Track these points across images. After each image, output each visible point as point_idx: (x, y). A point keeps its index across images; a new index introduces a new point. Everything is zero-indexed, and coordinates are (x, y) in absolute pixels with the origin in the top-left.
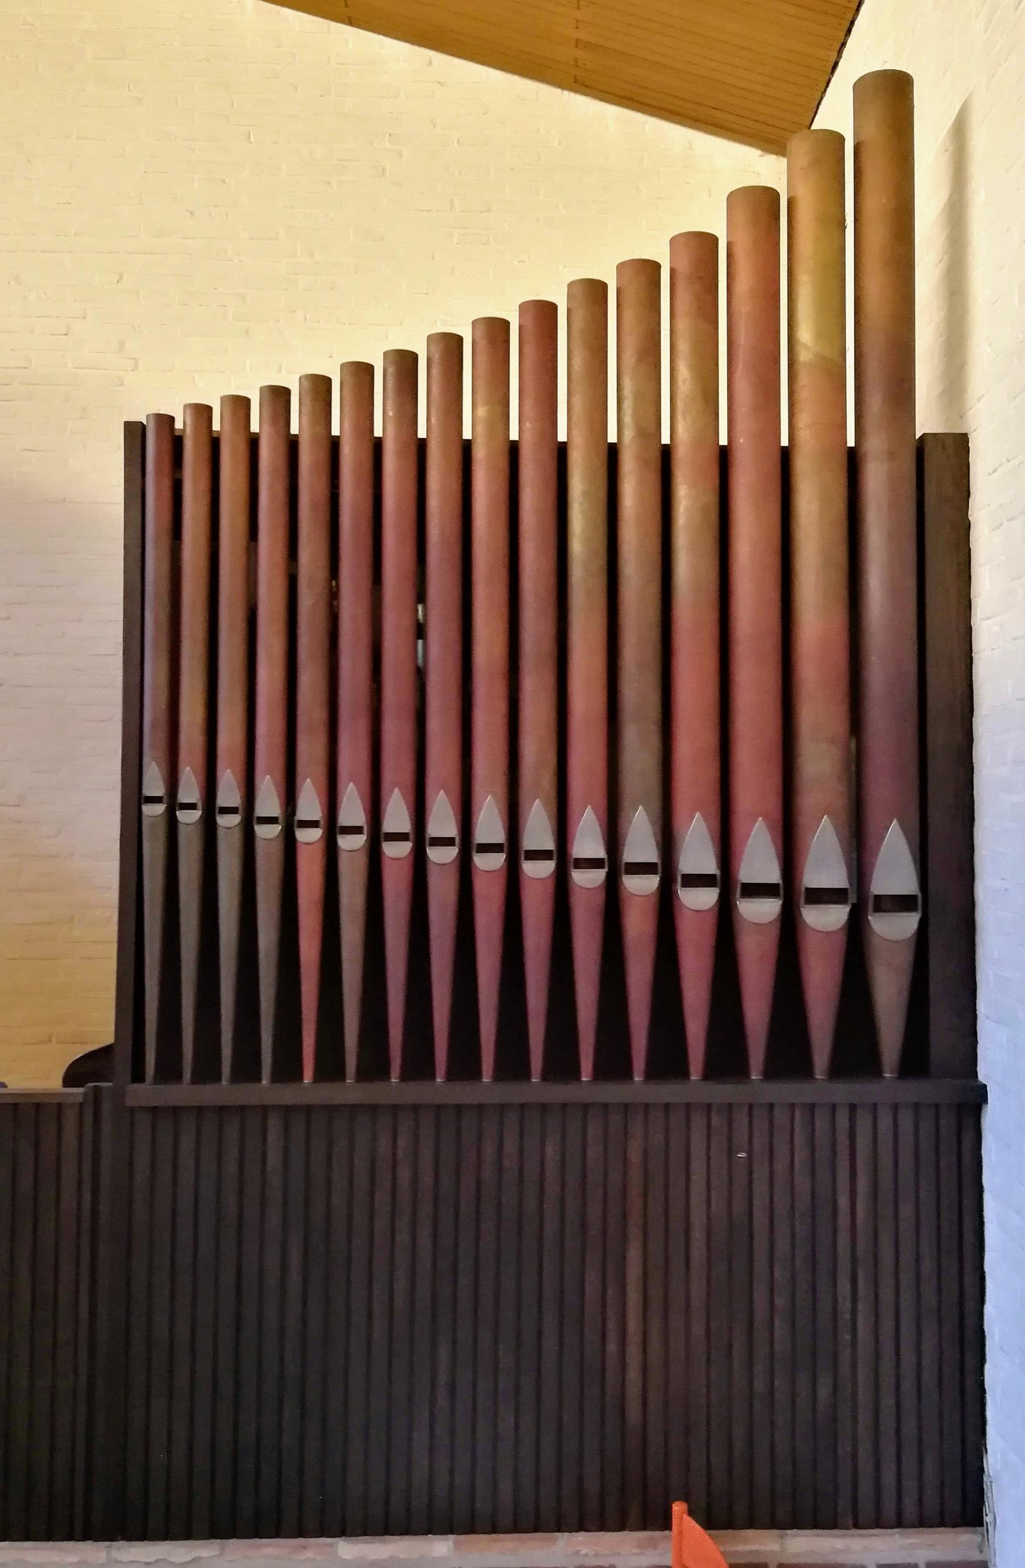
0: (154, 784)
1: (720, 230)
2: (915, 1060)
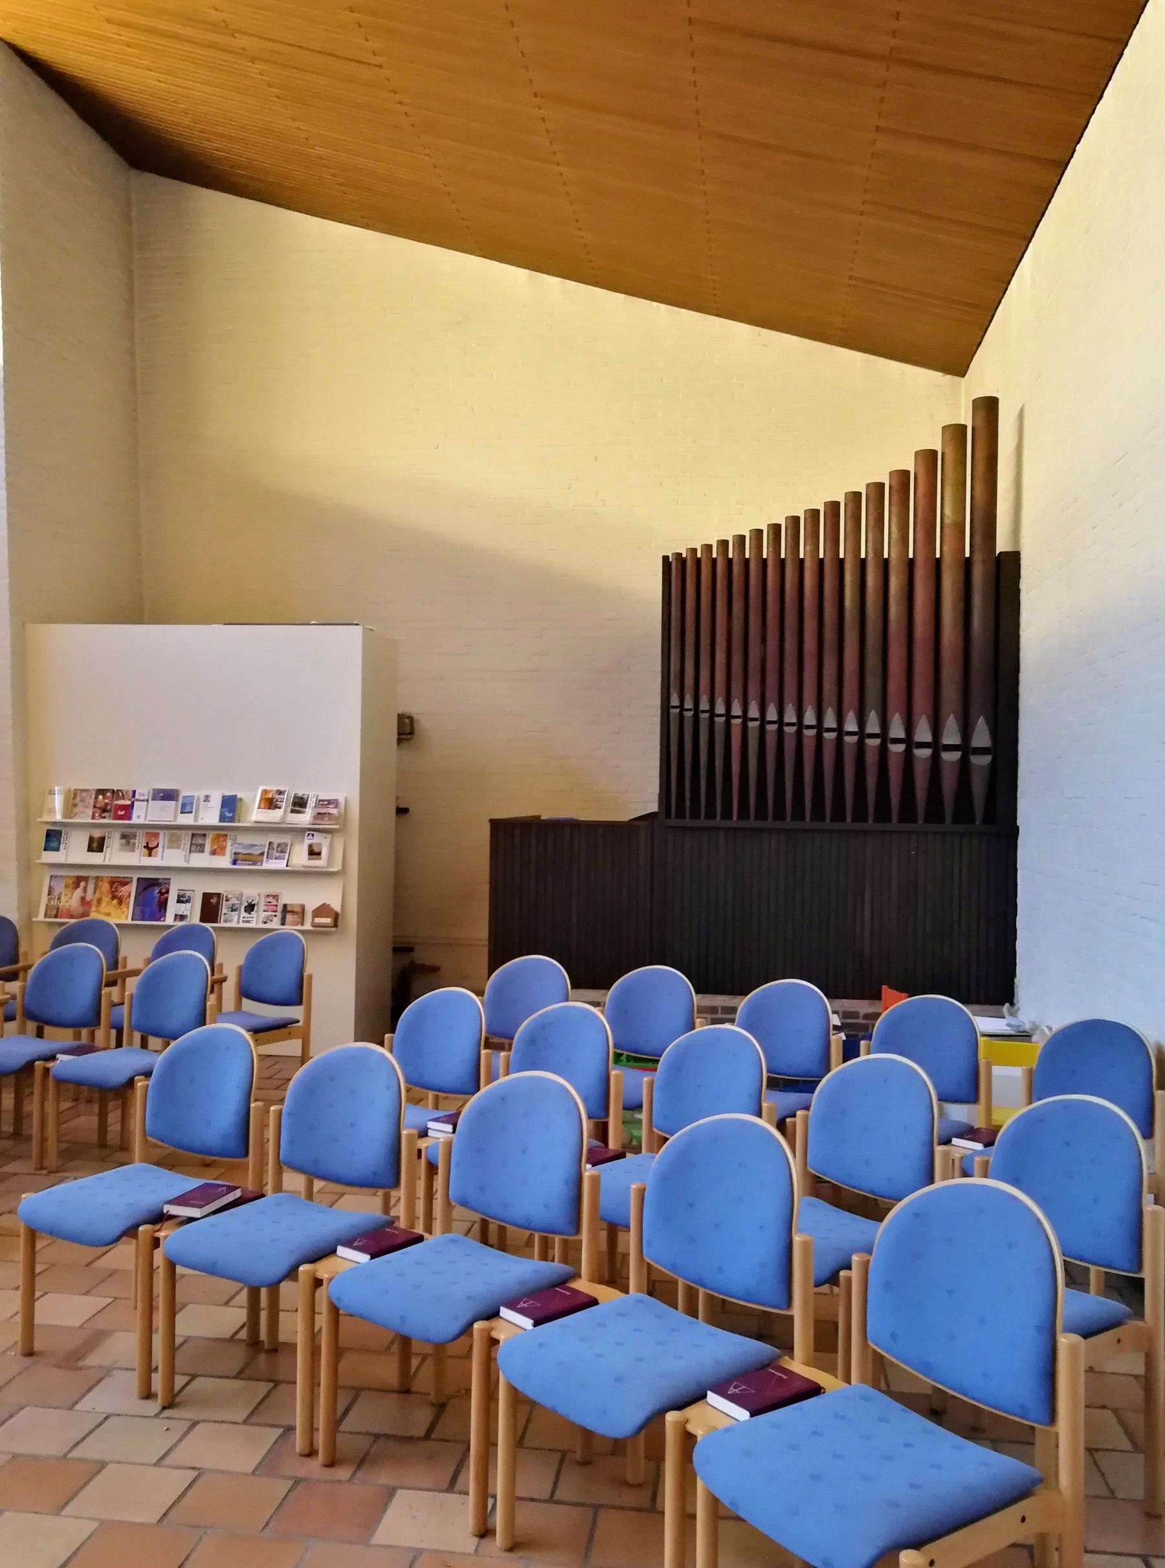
0: (675, 701)
1: (938, 448)
2: (990, 816)
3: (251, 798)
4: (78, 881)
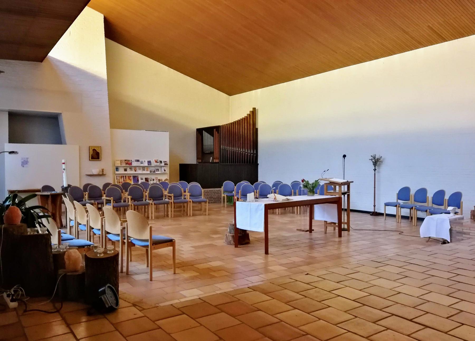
4: (122, 177)
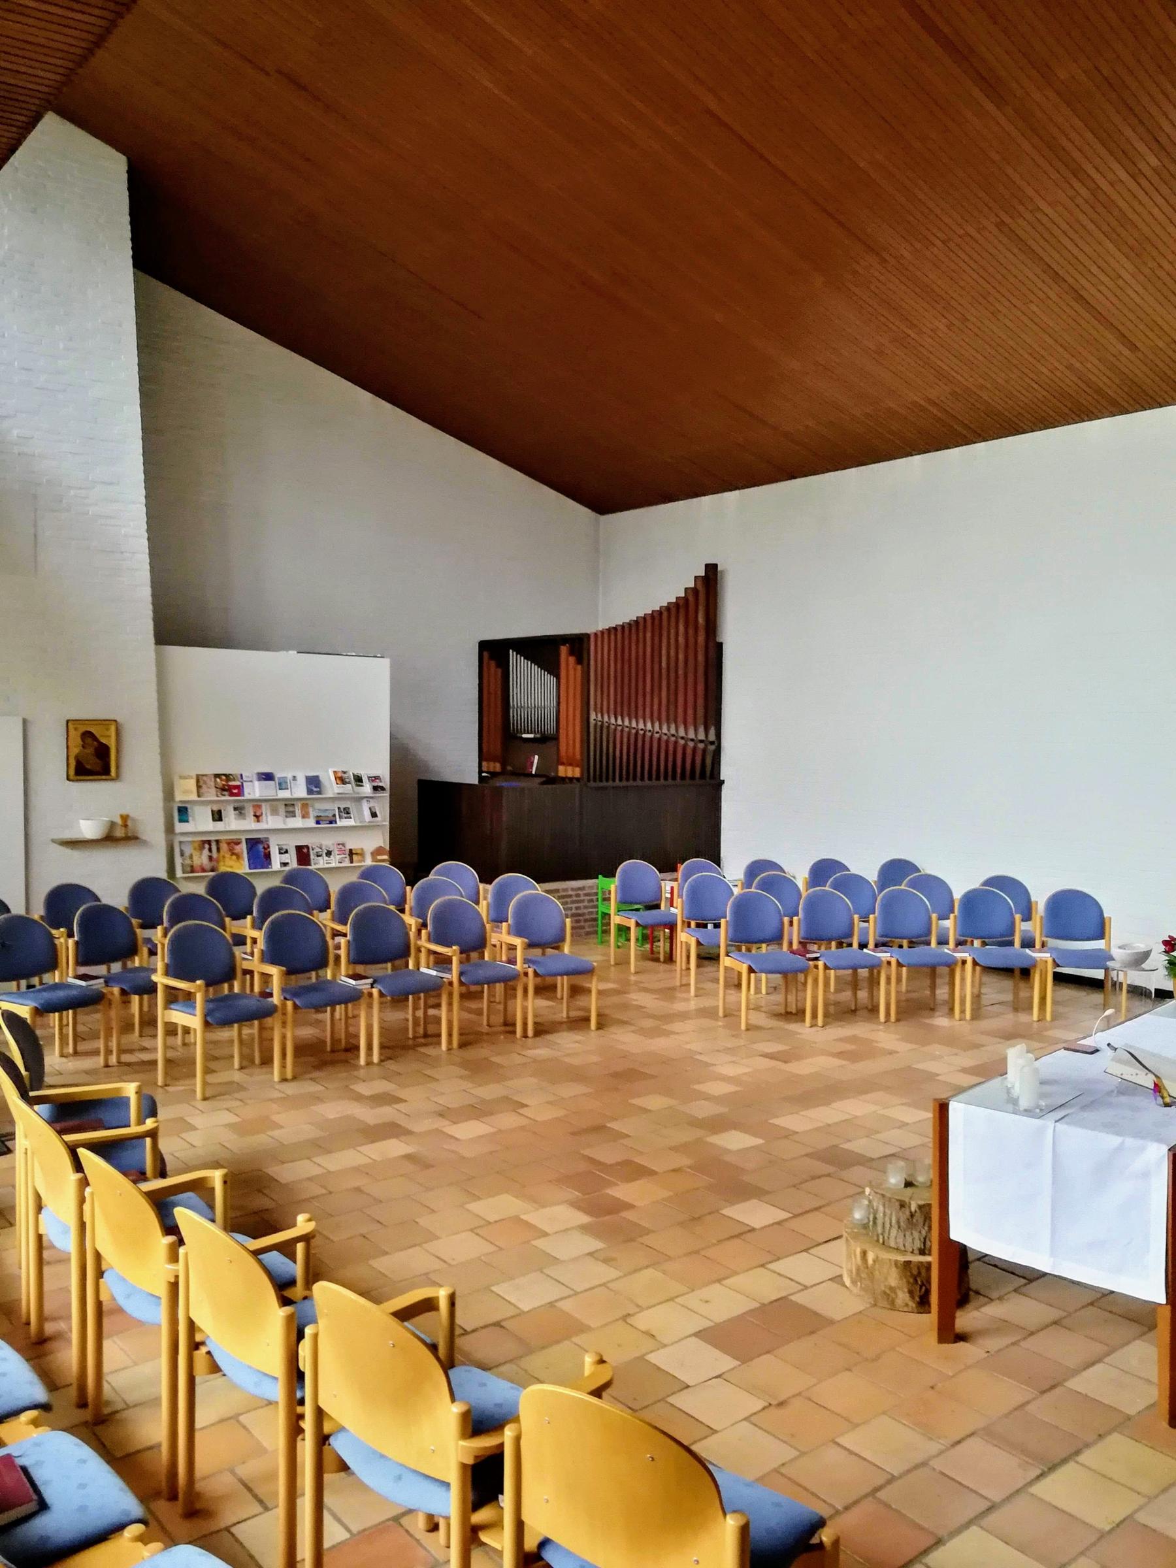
3: (328, 779)
